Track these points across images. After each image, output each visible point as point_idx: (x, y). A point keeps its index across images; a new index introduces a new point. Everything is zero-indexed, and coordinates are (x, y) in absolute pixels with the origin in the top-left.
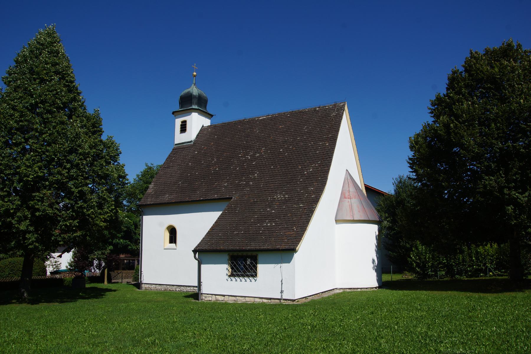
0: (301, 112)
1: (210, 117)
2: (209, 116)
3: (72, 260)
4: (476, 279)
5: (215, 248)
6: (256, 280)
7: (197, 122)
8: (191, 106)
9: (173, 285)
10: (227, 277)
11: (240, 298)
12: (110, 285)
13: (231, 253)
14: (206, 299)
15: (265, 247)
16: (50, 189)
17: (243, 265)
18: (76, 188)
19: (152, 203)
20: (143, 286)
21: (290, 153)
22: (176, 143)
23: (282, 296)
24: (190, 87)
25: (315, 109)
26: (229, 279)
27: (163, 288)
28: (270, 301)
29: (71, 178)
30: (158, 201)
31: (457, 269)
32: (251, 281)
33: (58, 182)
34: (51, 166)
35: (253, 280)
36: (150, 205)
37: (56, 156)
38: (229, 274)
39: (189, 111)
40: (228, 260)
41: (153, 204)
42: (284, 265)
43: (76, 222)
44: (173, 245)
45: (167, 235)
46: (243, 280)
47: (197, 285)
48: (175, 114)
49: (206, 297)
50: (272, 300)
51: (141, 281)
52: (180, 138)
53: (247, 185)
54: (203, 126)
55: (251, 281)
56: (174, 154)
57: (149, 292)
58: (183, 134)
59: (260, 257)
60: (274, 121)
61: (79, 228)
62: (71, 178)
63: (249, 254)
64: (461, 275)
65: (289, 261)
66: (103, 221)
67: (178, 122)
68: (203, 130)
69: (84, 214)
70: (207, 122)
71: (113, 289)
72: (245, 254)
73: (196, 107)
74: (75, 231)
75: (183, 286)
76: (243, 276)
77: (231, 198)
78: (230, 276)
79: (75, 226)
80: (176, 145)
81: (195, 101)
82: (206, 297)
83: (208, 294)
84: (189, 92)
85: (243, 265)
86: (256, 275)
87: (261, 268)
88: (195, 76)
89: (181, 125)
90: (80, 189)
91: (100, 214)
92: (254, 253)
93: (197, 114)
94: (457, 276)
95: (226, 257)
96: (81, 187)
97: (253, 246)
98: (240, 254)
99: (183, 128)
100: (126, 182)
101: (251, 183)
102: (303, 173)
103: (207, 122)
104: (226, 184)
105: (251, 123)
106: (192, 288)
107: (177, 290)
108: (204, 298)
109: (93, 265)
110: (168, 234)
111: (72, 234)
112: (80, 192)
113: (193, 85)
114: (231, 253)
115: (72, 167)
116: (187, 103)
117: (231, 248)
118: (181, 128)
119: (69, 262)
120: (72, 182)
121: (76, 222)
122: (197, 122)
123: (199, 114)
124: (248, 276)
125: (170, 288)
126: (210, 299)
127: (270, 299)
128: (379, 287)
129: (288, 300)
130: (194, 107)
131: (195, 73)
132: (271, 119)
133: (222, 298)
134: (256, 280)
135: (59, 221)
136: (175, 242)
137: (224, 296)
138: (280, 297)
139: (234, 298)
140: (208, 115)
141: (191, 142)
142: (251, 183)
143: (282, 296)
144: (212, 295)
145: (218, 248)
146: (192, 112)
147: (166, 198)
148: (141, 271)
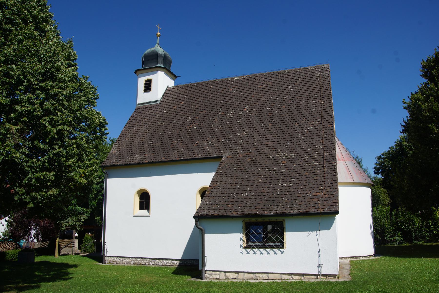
0: (280, 73)
1: (174, 78)
2: (174, 76)
3: (7, 229)
4: (435, 244)
5: (225, 213)
6: (282, 253)
7: (162, 82)
8: (157, 64)
9: (145, 258)
10: (242, 249)
11: (260, 275)
12: (62, 258)
13: (247, 220)
14: (211, 277)
15: (301, 211)
16: (16, 125)
17: (264, 232)
18: (53, 126)
19: (119, 164)
20: (107, 259)
21: (280, 112)
22: (139, 102)
23: (320, 271)
24: (154, 46)
25: (296, 71)
26: (245, 252)
27: (132, 261)
28: (302, 278)
29: (47, 113)
30: (127, 161)
31: (416, 235)
32: (275, 253)
33: (29, 113)
34: (17, 92)
35: (279, 252)
36: (117, 165)
37: (25, 77)
38: (245, 245)
39: (155, 69)
40: (243, 228)
41: (120, 165)
42: (322, 233)
43: (51, 175)
44: (145, 212)
45: (138, 200)
46: (265, 252)
47: (323, 272)
48: (138, 72)
49: (211, 275)
50: (306, 277)
51: (104, 254)
52: (143, 97)
53: (237, 143)
54: (168, 87)
55: (275, 253)
56: (138, 113)
57: (114, 267)
58: (148, 94)
59: (288, 223)
60: (249, 83)
61: (55, 184)
62: (47, 113)
63: (273, 219)
64: (418, 240)
65: (328, 227)
66: (83, 177)
67: (142, 81)
68: (168, 90)
69: (60, 163)
70: (171, 83)
71: (71, 263)
72: (267, 219)
73: (162, 66)
74: (48, 188)
75: (159, 259)
76: (264, 247)
77: (222, 157)
78: (245, 248)
79: (49, 181)
80: (139, 104)
81: (160, 60)
82: (211, 275)
83: (213, 271)
84: (153, 51)
85: (264, 232)
86: (283, 246)
87: (289, 237)
88: (159, 36)
89: (145, 84)
90: (60, 127)
91: (79, 167)
92: (280, 219)
93: (163, 73)
94: (415, 242)
95: (240, 224)
96: (60, 125)
97: (277, 210)
98: (260, 220)
99: (148, 87)
100: (106, 132)
101: (241, 141)
102: (302, 131)
103: (171, 83)
104: (210, 143)
105: (225, 83)
106: (170, 262)
107: (151, 263)
108: (208, 276)
109: (30, 234)
110: (139, 199)
111: (46, 192)
112: (59, 132)
113: (157, 45)
114: (247, 220)
115: (47, 98)
116: (151, 62)
117: (247, 213)
118: (145, 87)
119: (4, 231)
120: (47, 119)
121: (51, 175)
122: (162, 82)
123: (165, 73)
124: (272, 247)
125: (140, 261)
126: (218, 277)
127: (303, 275)
128: (375, 255)
129: (329, 275)
130: (159, 65)
131: (159, 33)
132: (248, 79)
133: (235, 275)
134: (282, 253)
135: (27, 173)
136: (148, 208)
137: (237, 273)
138: (317, 273)
139: (252, 275)
140: (171, 75)
141: (157, 101)
142: (241, 141)
143: (320, 271)
144: (220, 271)
145: (229, 213)
146: (158, 71)
147: (136, 158)
148: (104, 242)
